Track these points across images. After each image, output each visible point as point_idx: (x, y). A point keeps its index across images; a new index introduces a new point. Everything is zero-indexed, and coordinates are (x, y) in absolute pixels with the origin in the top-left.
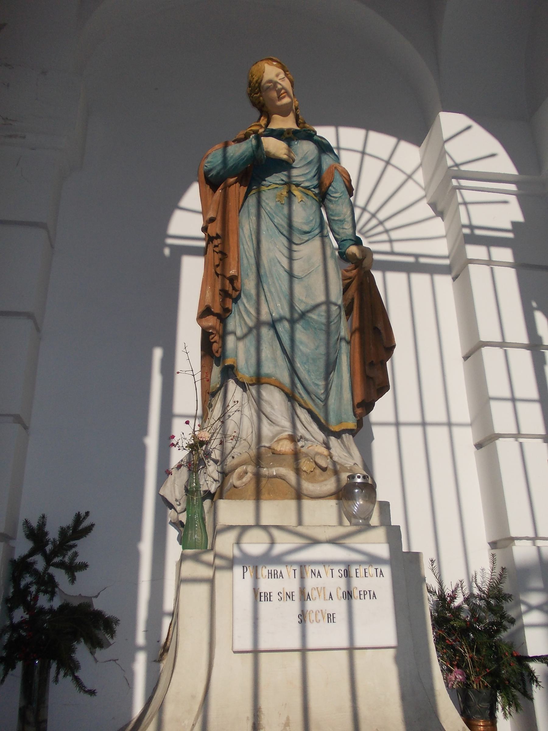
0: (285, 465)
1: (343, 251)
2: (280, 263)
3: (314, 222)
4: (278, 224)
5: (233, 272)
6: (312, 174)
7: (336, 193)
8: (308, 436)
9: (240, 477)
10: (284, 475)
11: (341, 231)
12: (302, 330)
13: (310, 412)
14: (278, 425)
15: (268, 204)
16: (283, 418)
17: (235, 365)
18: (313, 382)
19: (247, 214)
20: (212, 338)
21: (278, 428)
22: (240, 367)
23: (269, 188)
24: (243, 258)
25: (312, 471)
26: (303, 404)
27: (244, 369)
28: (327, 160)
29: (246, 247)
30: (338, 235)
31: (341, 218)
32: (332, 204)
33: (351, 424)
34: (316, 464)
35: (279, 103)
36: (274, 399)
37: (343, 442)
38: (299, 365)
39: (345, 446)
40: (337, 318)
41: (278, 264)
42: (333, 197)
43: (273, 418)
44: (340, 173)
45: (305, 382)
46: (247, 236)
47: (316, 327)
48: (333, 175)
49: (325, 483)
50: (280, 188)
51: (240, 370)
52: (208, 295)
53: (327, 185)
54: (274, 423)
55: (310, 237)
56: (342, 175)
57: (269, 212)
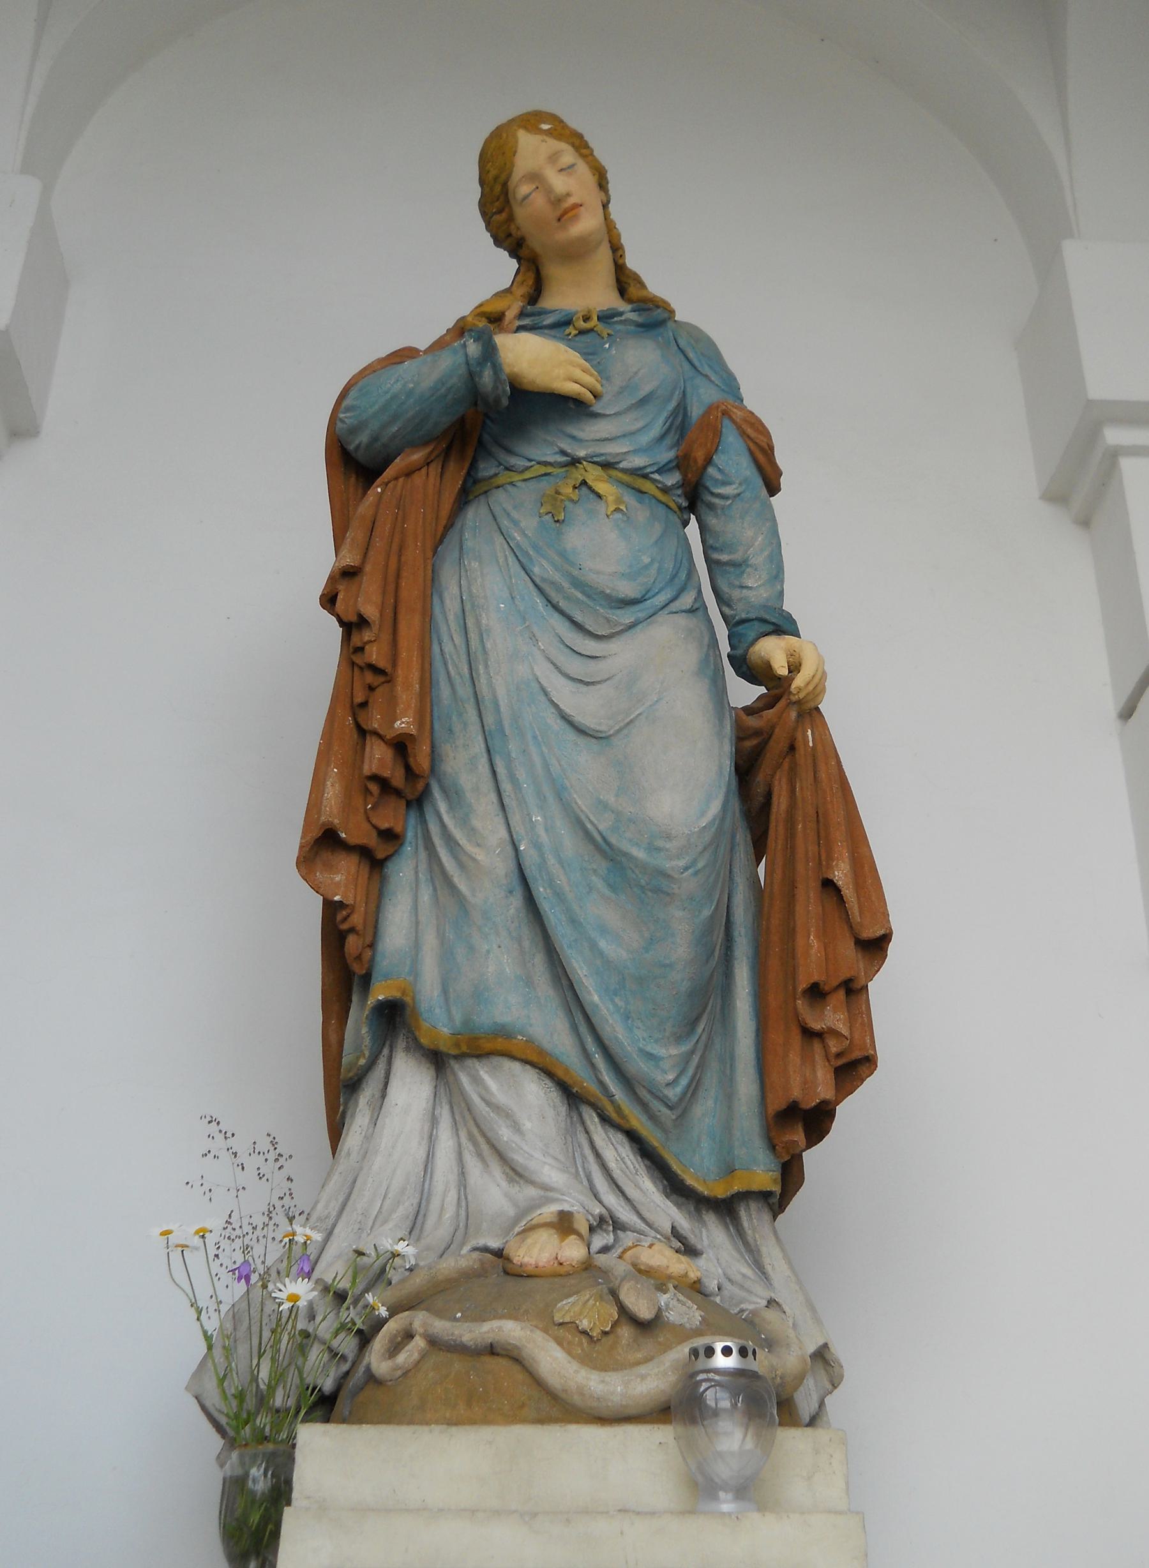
0: (527, 1312)
1: (739, 652)
2: (546, 694)
3: (653, 571)
4: (544, 580)
5: (403, 724)
6: (656, 430)
7: (725, 483)
8: (625, 1214)
9: (394, 1349)
10: (516, 1347)
11: (736, 594)
12: (607, 892)
13: (633, 1137)
14: (532, 1183)
15: (516, 523)
16: (550, 1160)
17: (408, 999)
18: (641, 1050)
19: (456, 554)
20: (345, 919)
21: (532, 1192)
22: (423, 1007)
23: (527, 475)
24: (438, 683)
25: (605, 1333)
26: (614, 1116)
27: (437, 1011)
28: (702, 391)
29: (448, 648)
30: (729, 606)
31: (737, 557)
32: (716, 516)
33: (763, 1174)
34: (623, 1309)
35: (561, 236)
36: (524, 1103)
37: (741, 1233)
38: (596, 998)
39: (746, 1244)
40: (707, 855)
41: (543, 698)
42: (719, 496)
43: (518, 1158)
44: (739, 427)
45: (614, 1049)
46: (451, 617)
47: (643, 882)
48: (718, 434)
49: (642, 1369)
50: (557, 476)
51: (425, 1015)
52: (332, 792)
53: (700, 462)
54: (520, 1176)
55: (641, 615)
56: (743, 434)
57: (518, 545)
